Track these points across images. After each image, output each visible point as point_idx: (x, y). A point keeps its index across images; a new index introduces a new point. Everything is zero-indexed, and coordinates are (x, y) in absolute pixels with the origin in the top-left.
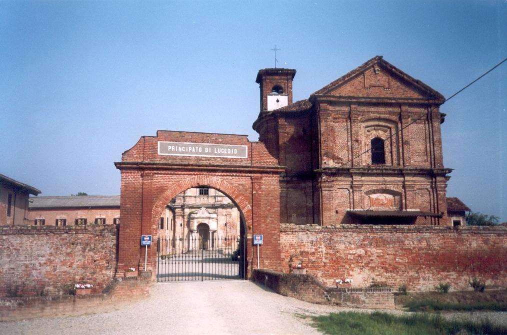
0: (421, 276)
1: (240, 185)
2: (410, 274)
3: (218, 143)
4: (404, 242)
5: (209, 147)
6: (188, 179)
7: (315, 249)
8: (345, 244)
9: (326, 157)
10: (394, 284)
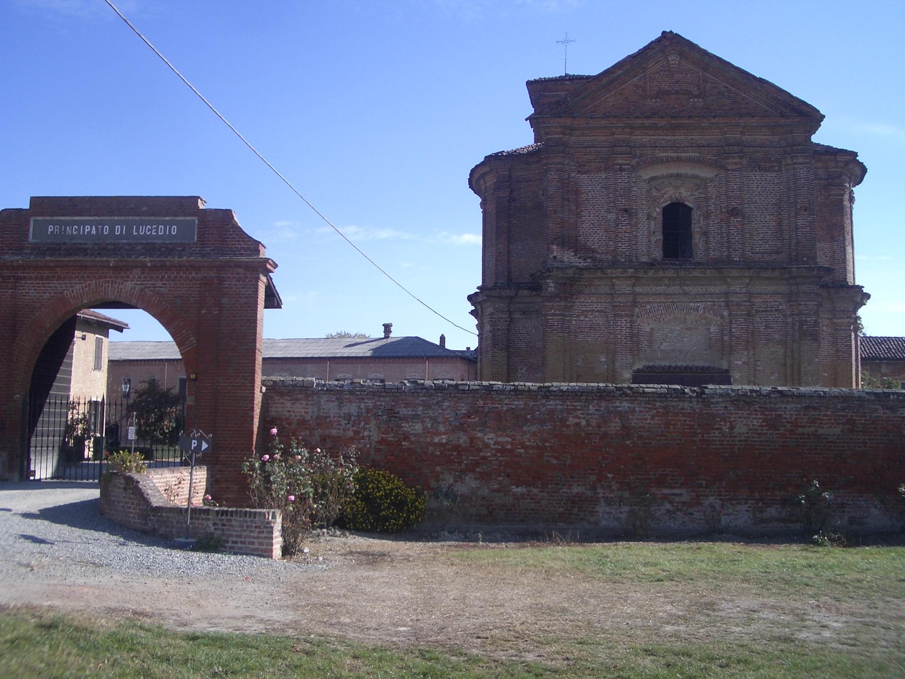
0: (601, 495)
1: (176, 297)
2: (575, 491)
3: (139, 215)
4: (567, 420)
5: (121, 223)
6: (78, 286)
7: (354, 431)
8: (423, 422)
9: (558, 245)
10: (533, 510)
